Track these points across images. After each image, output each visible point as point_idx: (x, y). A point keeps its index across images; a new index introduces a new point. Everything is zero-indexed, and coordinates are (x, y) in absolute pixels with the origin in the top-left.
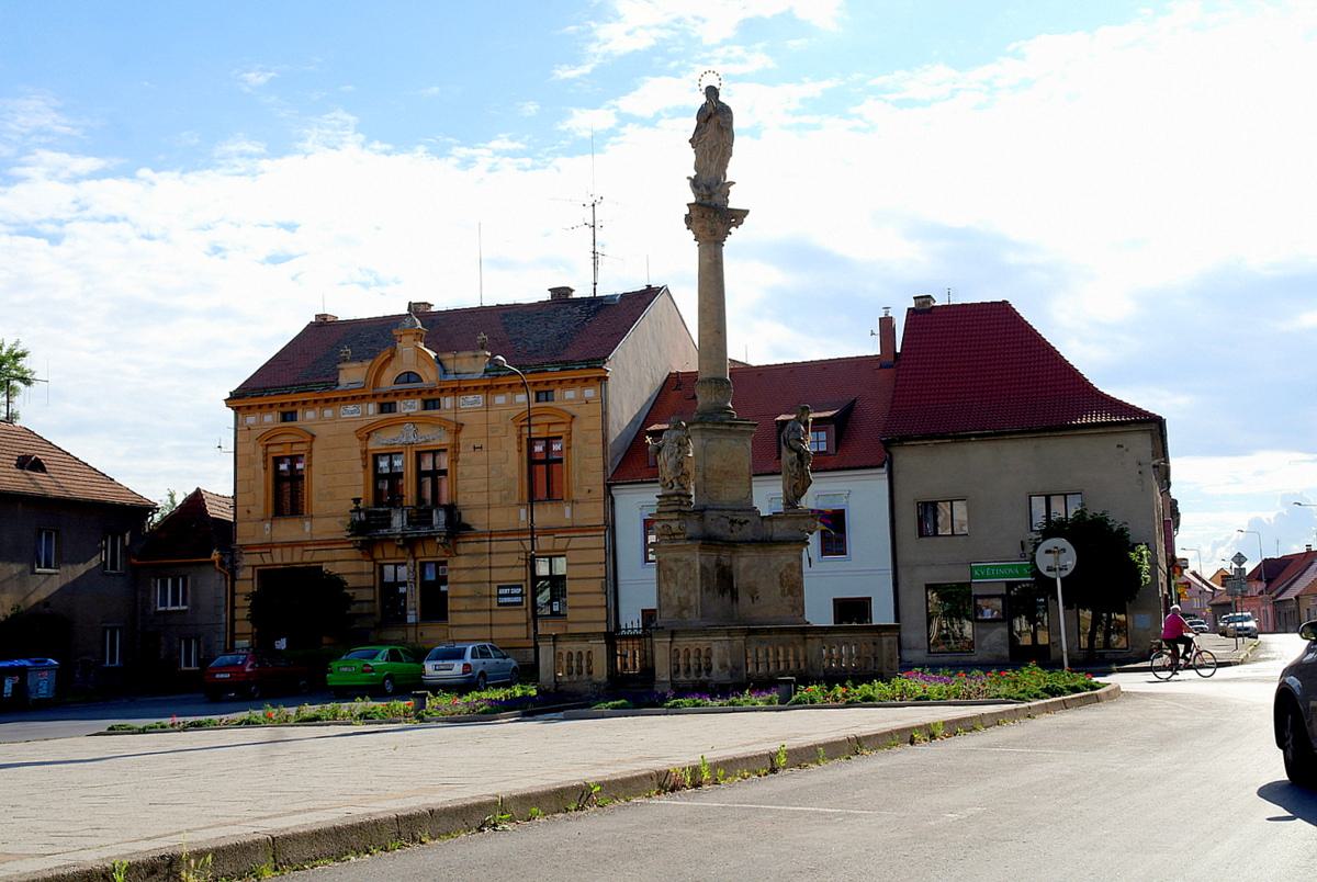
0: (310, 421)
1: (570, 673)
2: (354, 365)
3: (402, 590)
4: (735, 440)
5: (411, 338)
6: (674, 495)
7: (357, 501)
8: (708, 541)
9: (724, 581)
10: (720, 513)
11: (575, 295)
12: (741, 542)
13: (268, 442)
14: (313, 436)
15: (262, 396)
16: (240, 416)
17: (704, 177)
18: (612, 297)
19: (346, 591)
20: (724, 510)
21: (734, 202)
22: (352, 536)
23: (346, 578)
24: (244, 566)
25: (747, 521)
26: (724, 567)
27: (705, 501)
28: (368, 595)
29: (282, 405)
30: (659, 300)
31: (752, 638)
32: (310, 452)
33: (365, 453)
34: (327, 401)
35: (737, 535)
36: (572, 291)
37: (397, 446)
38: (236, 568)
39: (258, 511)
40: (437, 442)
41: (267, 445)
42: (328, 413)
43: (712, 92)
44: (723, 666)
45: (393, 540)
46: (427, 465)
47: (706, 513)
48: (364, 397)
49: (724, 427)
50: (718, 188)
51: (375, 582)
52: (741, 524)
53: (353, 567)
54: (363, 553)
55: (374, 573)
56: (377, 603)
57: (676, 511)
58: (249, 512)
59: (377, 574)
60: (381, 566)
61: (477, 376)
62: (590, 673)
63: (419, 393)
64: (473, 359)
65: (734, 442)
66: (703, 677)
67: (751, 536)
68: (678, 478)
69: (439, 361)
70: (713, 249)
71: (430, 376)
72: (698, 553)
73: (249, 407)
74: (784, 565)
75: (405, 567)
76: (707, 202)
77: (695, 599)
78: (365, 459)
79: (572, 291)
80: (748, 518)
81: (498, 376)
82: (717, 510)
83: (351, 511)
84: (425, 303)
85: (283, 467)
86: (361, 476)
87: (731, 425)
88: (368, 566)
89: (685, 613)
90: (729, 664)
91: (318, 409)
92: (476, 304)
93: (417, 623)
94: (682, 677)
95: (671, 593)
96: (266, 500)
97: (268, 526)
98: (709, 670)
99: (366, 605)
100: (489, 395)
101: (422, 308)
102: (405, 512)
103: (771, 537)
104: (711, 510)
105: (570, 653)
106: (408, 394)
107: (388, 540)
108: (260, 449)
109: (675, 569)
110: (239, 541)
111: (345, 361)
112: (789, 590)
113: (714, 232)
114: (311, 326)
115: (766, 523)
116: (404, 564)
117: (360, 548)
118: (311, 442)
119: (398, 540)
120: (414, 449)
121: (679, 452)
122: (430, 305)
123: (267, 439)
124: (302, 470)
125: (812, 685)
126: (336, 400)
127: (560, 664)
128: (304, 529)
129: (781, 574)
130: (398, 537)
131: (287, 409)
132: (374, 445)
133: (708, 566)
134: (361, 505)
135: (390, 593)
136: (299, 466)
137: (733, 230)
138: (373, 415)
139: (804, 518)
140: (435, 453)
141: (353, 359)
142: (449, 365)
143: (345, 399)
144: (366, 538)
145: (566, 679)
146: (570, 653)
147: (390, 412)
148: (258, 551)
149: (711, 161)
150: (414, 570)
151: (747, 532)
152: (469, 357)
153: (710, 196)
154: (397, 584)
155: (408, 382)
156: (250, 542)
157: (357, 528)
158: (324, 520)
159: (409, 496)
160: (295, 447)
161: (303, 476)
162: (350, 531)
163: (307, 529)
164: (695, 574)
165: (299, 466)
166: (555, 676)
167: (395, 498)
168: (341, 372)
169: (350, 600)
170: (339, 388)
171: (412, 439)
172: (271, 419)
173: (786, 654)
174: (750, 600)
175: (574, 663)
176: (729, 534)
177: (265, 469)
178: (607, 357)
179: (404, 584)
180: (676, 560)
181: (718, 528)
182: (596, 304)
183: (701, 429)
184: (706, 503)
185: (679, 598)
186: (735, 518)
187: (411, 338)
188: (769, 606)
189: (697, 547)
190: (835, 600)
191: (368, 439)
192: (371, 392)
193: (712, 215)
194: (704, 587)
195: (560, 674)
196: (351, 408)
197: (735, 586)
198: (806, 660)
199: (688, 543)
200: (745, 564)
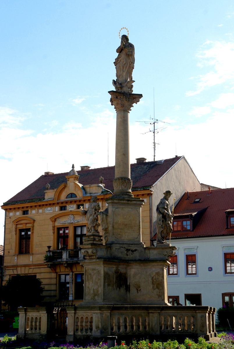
0: (34, 214)
1: (32, 329)
2: (51, 191)
3: (68, 285)
4: (132, 208)
5: (72, 179)
6: (90, 236)
7: (49, 247)
8: (108, 260)
9: (121, 281)
10: (121, 245)
11: (147, 161)
12: (131, 260)
13: (17, 223)
14: (34, 221)
15: (15, 204)
16: (7, 213)
17: (120, 80)
18: (160, 161)
19: (42, 286)
20: (124, 244)
21: (135, 91)
22: (46, 262)
23: (42, 280)
24: (6, 275)
25: (136, 250)
26: (121, 274)
27: (111, 239)
28: (53, 288)
29: (23, 208)
30: (179, 162)
31: (116, 312)
32: (33, 227)
33: (54, 227)
34: (40, 206)
35: (131, 256)
36: (145, 159)
37: (66, 224)
38: (3, 276)
39: (13, 252)
40: (82, 223)
41: (17, 225)
42: (40, 211)
43: (125, 38)
44: (97, 327)
45: (62, 264)
46: (79, 232)
47: (113, 245)
48: (54, 204)
49: (124, 202)
50: (126, 84)
51: (56, 282)
52: (133, 251)
53: (48, 276)
54: (52, 269)
55: (56, 278)
56: (57, 291)
57: (90, 244)
58: (9, 252)
59: (58, 279)
60: (60, 275)
61: (98, 194)
62: (40, 329)
63: (75, 202)
64: (97, 187)
65: (130, 209)
66: (89, 333)
67: (138, 258)
68: (94, 227)
69: (83, 188)
70: (122, 114)
71: (80, 195)
72: (102, 266)
73: (10, 209)
74: (154, 274)
75: (69, 276)
76: (120, 91)
77: (101, 290)
78: (54, 230)
79: (145, 159)
80: (137, 248)
81: (107, 194)
82: (119, 244)
83: (47, 252)
84: (87, 166)
85: (23, 233)
86: (52, 237)
87: (128, 200)
88: (54, 275)
89: (96, 297)
90: (100, 326)
91: (36, 209)
92: (106, 166)
93: (73, 300)
94: (79, 333)
95: (90, 287)
96: (16, 247)
97: (16, 258)
98: (91, 329)
99: (53, 292)
100: (104, 202)
101: (85, 168)
102: (68, 252)
103: (149, 259)
104: (116, 244)
105: (32, 318)
106: (71, 202)
107: (60, 264)
108: (14, 226)
109: (92, 274)
110: (5, 264)
111: (47, 189)
112: (157, 286)
113: (123, 106)
114: (42, 177)
115: (147, 251)
116: (68, 274)
117: (50, 268)
118: (34, 223)
119: (65, 264)
120: (73, 226)
121: (95, 213)
122: (89, 167)
123: (17, 222)
124: (30, 234)
125: (142, 340)
126: (43, 205)
127: (28, 325)
128: (30, 260)
129: (153, 278)
130: (65, 263)
131: (25, 209)
132: (58, 224)
133: (110, 273)
134: (51, 249)
135: (63, 286)
136: (29, 233)
137: (134, 104)
138: (57, 212)
139: (166, 248)
140: (82, 227)
141: (50, 189)
142: (88, 190)
143: (46, 205)
144: (52, 263)
145: (30, 332)
146: (32, 318)
147: (64, 210)
148: (12, 268)
149: (123, 71)
150: (72, 277)
151: (137, 255)
152: (96, 186)
153: (121, 88)
154: (66, 283)
155: (72, 197)
156: (9, 265)
157: (48, 259)
158: (38, 256)
159: (71, 246)
160: (28, 225)
161: (30, 237)
162: (45, 260)
163: (31, 260)
164: (101, 276)
165: (29, 233)
166: (25, 330)
167: (65, 247)
168: (46, 194)
169: (42, 290)
170: (44, 200)
171: (72, 221)
172: (19, 214)
173: (138, 321)
174: (136, 291)
175: (34, 324)
176: (126, 256)
177: (16, 234)
178: (152, 185)
179: (68, 283)
180: (93, 270)
181: (118, 252)
182: (154, 164)
183: (112, 202)
184: (114, 240)
185: (93, 289)
186: (129, 248)
187: (72, 179)
188: (146, 295)
189: (102, 263)
190: (185, 294)
191: (55, 221)
192: (56, 202)
193: (122, 97)
194: (106, 284)
195: (28, 329)
196: (49, 209)
197: (128, 284)
198: (149, 325)
199: (98, 260)
200: (134, 273)
